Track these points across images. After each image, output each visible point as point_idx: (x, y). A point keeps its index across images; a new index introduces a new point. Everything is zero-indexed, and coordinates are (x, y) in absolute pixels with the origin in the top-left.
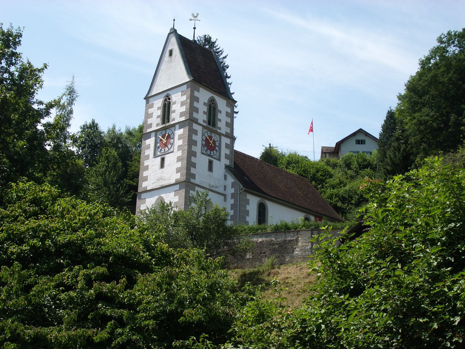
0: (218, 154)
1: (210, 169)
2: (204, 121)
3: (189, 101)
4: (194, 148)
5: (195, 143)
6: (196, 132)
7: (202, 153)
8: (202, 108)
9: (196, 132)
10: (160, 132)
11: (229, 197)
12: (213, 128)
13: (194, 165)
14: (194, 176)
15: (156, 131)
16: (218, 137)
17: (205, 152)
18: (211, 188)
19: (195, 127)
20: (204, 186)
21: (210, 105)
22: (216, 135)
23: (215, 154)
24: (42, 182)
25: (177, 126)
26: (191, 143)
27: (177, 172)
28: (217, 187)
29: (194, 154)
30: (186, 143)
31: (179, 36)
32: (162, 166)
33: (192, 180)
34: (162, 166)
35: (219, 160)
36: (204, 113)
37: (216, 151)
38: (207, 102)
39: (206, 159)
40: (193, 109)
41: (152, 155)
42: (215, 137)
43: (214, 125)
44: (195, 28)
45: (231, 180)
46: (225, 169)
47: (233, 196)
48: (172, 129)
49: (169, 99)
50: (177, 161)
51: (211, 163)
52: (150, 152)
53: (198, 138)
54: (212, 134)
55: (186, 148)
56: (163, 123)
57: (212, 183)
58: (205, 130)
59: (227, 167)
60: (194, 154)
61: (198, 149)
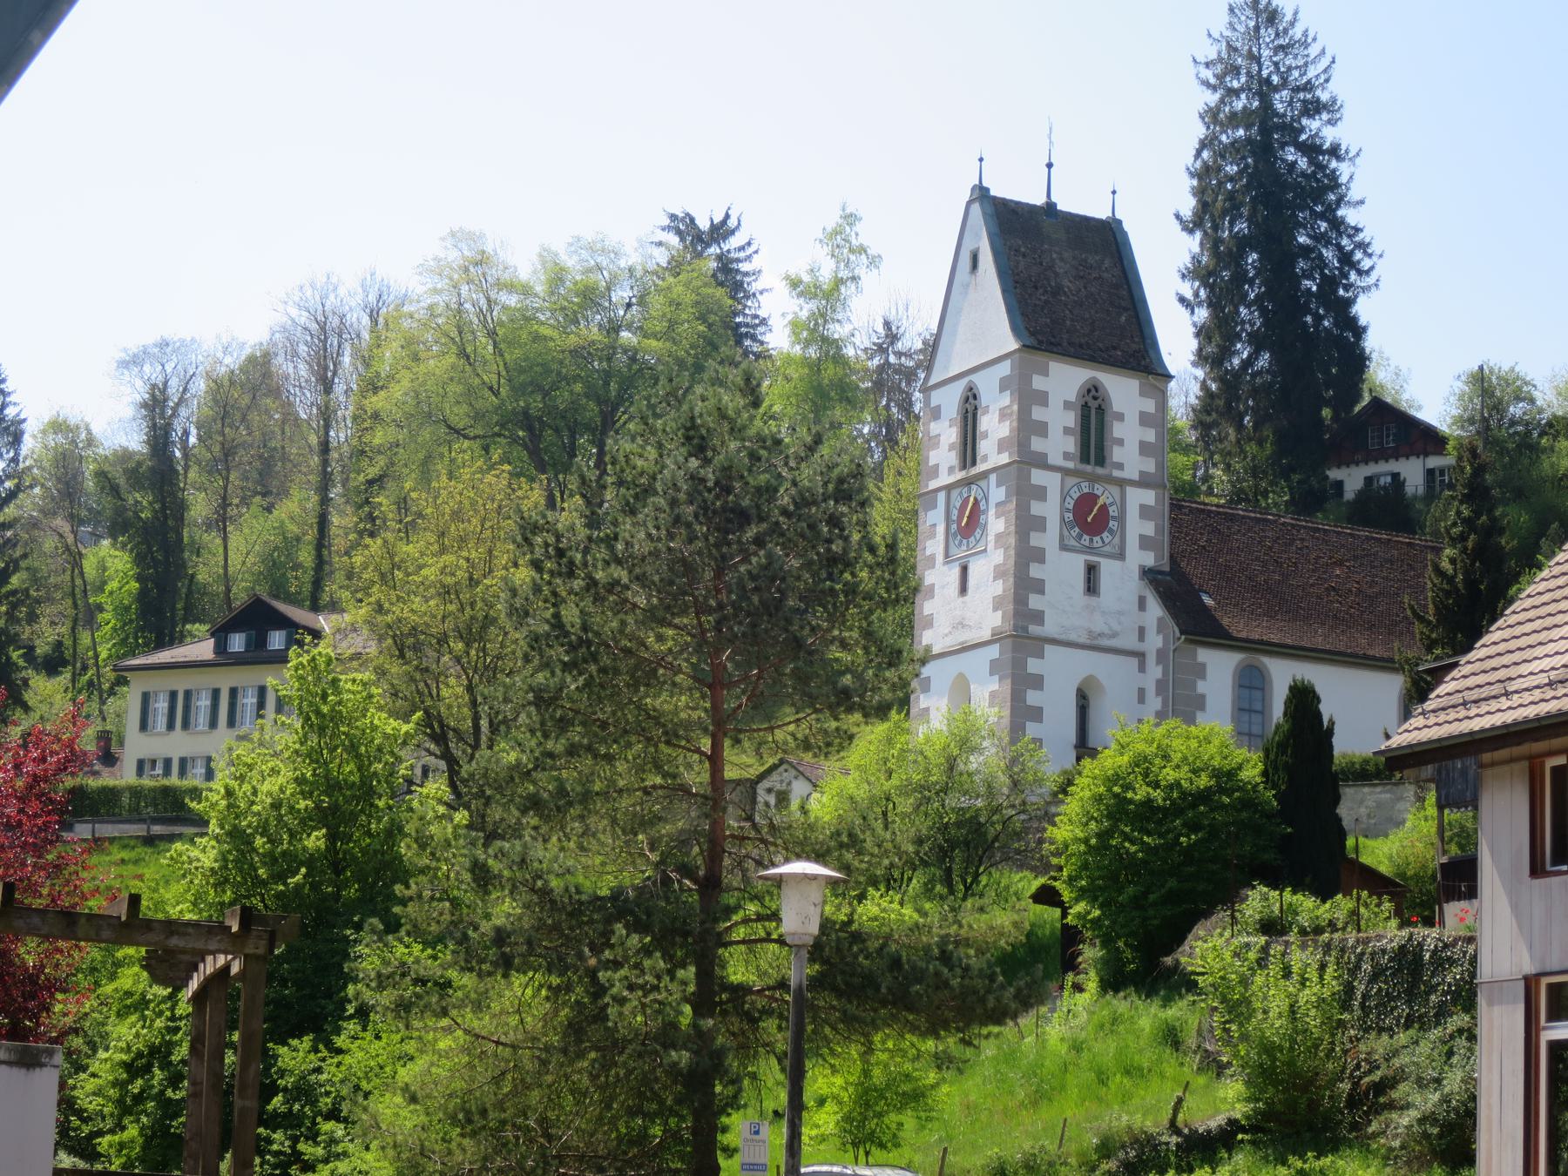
0: (1117, 540)
1: (1092, 587)
2: (1066, 456)
3: (1015, 407)
4: (1036, 540)
5: (1040, 524)
6: (1041, 493)
7: (1064, 547)
8: (1060, 420)
9: (1041, 493)
10: (958, 490)
11: (1151, 659)
12: (1099, 470)
13: (1039, 587)
14: (1038, 617)
15: (949, 488)
16: (1115, 490)
17: (1073, 542)
18: (1096, 642)
19: (1038, 477)
20: (1073, 637)
21: (1085, 406)
22: (1107, 486)
23: (1107, 541)
24: (1353, 1101)
25: (993, 478)
26: (1027, 525)
27: (995, 609)
28: (1114, 635)
29: (1039, 556)
30: (1013, 528)
31: (995, 205)
32: (963, 589)
33: (1034, 629)
34: (963, 589)
35: (1121, 556)
36: (1067, 431)
37: (1111, 532)
38: (1072, 398)
39: (1078, 562)
40: (1028, 428)
41: (940, 558)
42: (1106, 494)
43: (1101, 460)
44: (1050, 166)
45: (1155, 610)
46: (1141, 579)
47: (1161, 656)
48: (983, 483)
49: (975, 397)
50: (995, 578)
51: (1092, 571)
52: (934, 546)
53: (1051, 509)
54: (1096, 486)
55: (1012, 541)
56: (964, 467)
57: (1099, 625)
58: (1071, 481)
59: (1148, 574)
60: (1039, 556)
61: (1048, 539)
